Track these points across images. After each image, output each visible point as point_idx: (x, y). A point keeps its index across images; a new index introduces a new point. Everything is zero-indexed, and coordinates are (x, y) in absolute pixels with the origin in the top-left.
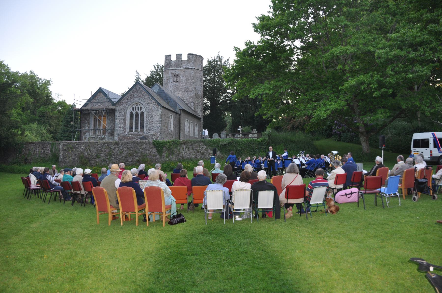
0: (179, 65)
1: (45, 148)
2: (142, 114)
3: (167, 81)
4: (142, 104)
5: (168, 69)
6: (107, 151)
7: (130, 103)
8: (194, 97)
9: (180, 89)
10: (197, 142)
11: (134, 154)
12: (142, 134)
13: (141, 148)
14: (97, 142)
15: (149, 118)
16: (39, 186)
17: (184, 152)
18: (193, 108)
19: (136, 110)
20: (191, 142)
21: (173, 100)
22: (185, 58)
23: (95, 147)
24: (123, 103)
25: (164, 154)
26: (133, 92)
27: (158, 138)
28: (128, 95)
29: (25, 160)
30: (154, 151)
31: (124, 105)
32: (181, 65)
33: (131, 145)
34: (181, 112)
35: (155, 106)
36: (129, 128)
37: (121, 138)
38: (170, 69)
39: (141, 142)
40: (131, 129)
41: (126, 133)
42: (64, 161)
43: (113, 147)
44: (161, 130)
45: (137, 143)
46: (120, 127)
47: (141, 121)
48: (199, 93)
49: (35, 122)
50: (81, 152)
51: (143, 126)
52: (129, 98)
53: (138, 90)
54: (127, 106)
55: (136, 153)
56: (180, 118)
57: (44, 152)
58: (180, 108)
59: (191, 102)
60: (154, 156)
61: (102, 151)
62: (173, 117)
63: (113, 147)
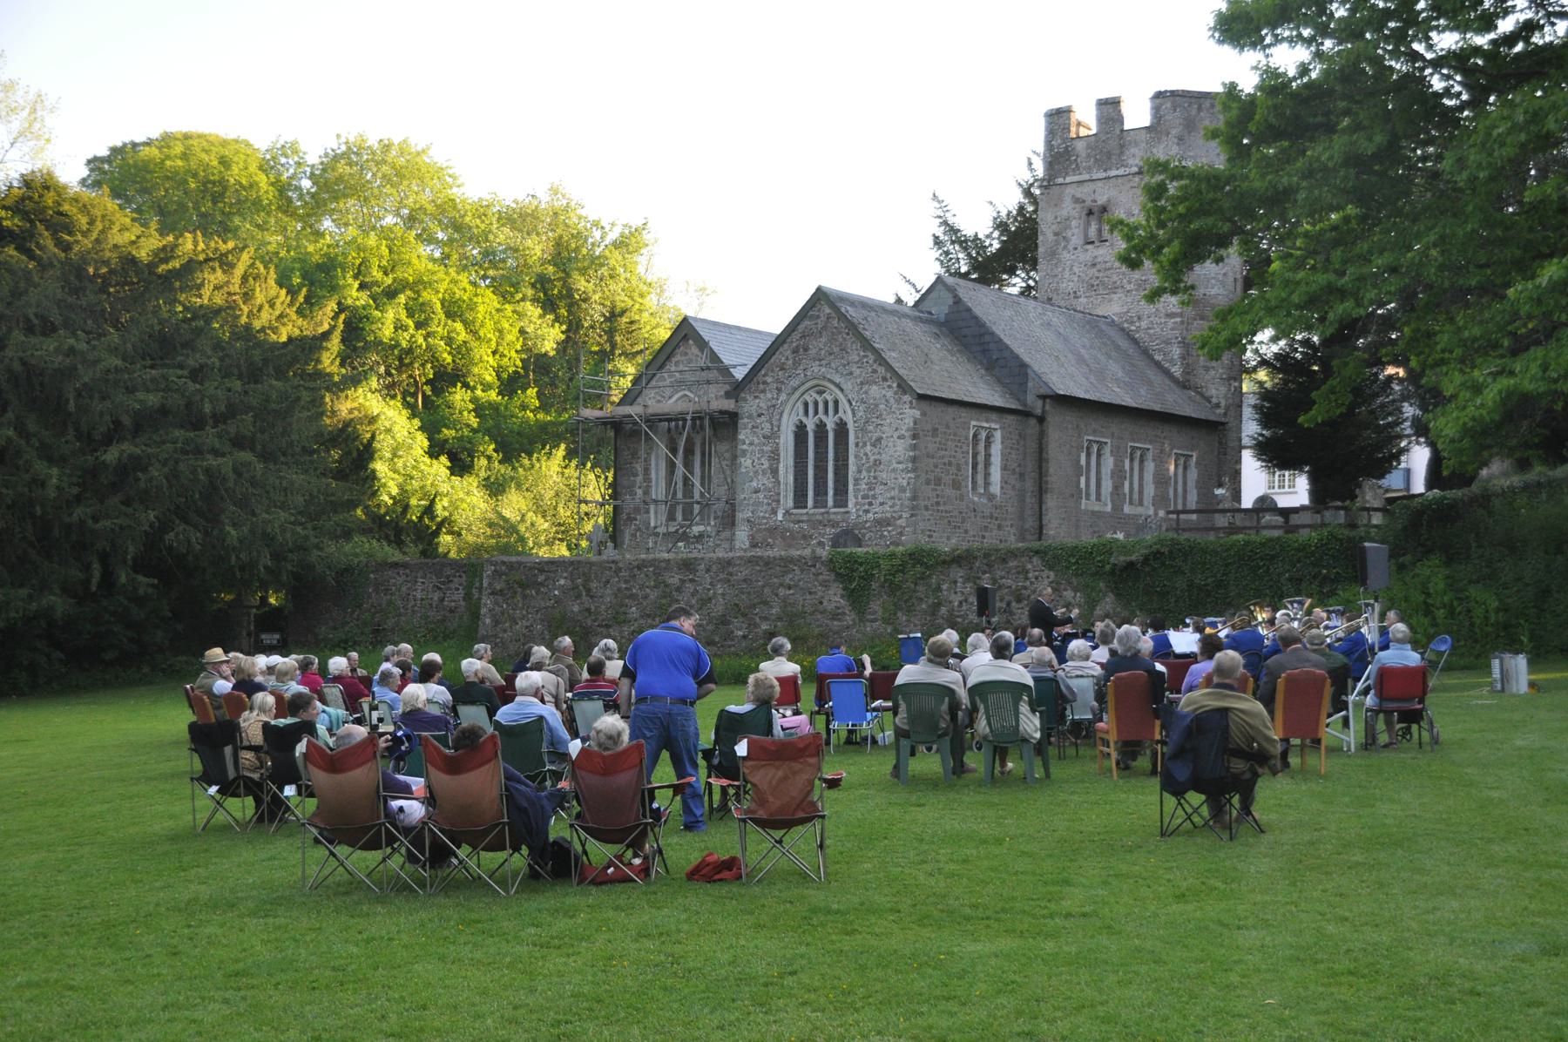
0: (1109, 155)
1: (443, 583)
2: (842, 429)
3: (1057, 243)
4: (838, 386)
5: (1060, 180)
6: (653, 595)
7: (794, 383)
8: (1181, 315)
9: (1115, 278)
10: (1013, 554)
11: (754, 606)
12: (820, 518)
13: (781, 585)
14: (613, 562)
15: (869, 448)
16: (1236, 800)
17: (956, 600)
18: (1177, 370)
19: (816, 412)
20: (986, 556)
21: (1012, 352)
22: (1137, 115)
23: (608, 582)
24: (765, 383)
25: (876, 606)
26: (803, 337)
27: (901, 534)
28: (786, 350)
29: (376, 632)
30: (834, 597)
31: (769, 396)
32: (1122, 153)
33: (744, 572)
34: (1048, 407)
35: (890, 394)
36: (791, 495)
37: (759, 537)
38: (1068, 179)
39: (781, 559)
40: (800, 499)
41: (780, 517)
42: (496, 636)
43: (674, 580)
44: (914, 498)
45: (767, 564)
46: (757, 491)
47: (836, 459)
48: (1213, 292)
49: (558, 446)
50: (558, 601)
51: (846, 485)
52: (790, 362)
53: (825, 328)
54: (783, 397)
55: (765, 603)
56: (1042, 435)
57: (442, 600)
58: (1043, 391)
59: (1168, 342)
60: (835, 616)
61: (632, 596)
62: (998, 435)
63: (674, 580)
